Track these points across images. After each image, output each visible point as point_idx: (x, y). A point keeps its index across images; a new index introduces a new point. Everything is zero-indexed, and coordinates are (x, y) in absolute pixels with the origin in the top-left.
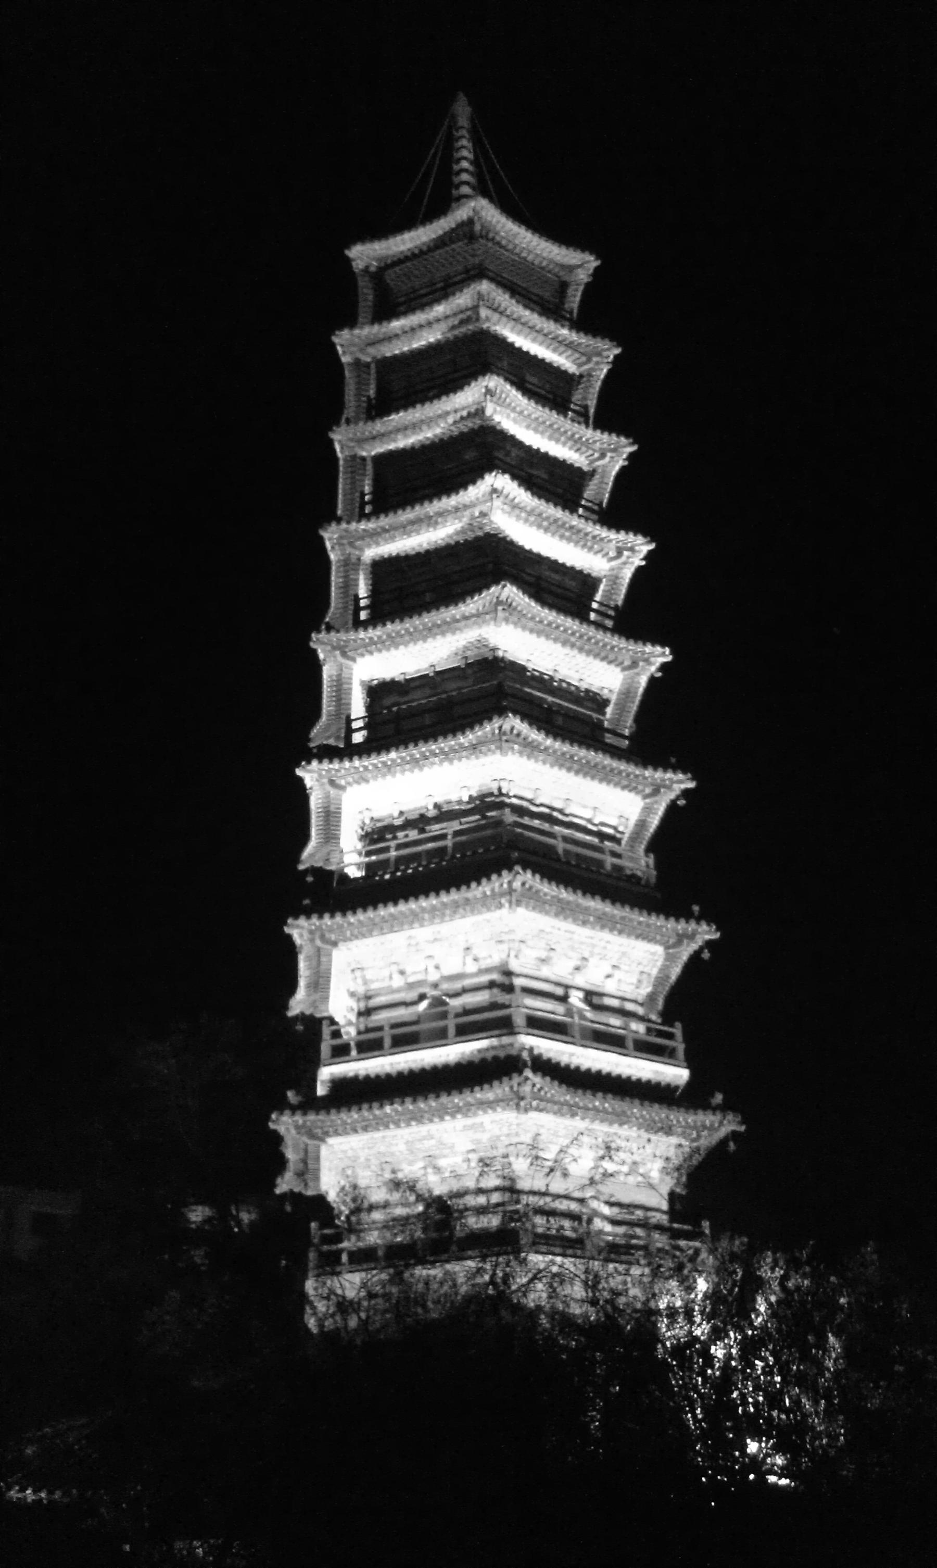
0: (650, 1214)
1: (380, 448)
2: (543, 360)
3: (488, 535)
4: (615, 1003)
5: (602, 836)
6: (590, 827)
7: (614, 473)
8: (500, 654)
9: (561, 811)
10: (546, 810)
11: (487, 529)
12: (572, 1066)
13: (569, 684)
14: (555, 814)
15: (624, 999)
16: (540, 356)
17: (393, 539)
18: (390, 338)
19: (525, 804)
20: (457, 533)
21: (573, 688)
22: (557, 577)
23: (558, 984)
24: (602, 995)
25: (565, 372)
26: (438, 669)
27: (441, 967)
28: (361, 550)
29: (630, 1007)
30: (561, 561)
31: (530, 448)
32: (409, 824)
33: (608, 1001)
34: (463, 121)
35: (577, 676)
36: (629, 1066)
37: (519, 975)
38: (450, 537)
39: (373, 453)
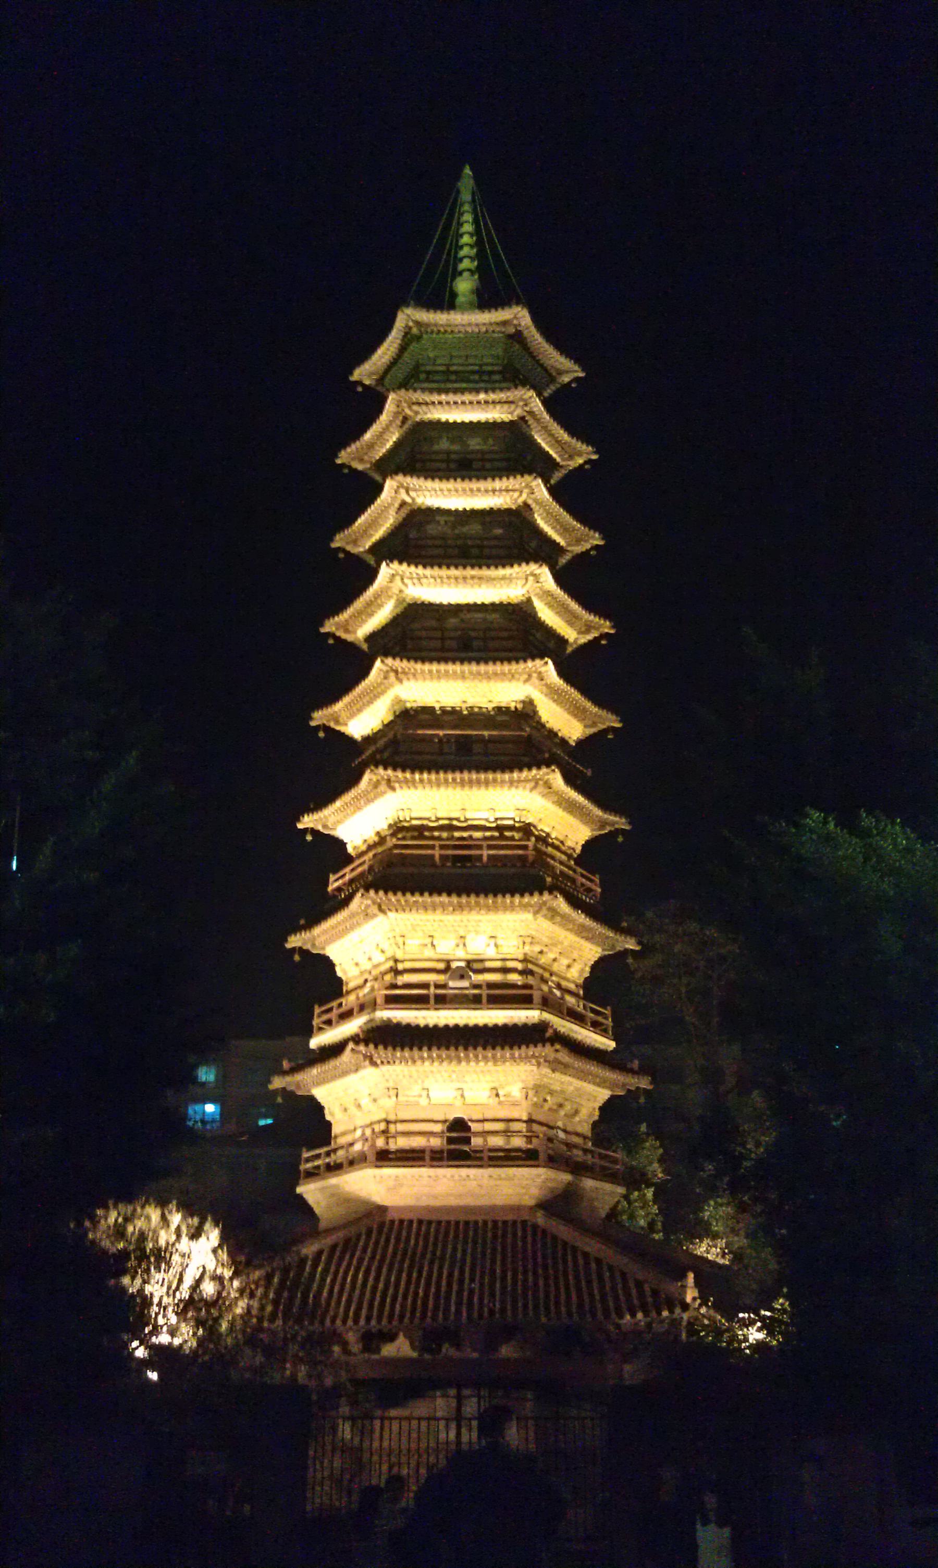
0: (511, 1124)
1: (368, 545)
2: (479, 422)
3: (410, 605)
4: (498, 964)
5: (501, 829)
6: (488, 825)
7: (548, 496)
8: (409, 705)
9: (458, 819)
10: (446, 822)
11: (408, 600)
12: (431, 1026)
13: (480, 708)
14: (455, 823)
15: (504, 960)
16: (475, 420)
17: (364, 621)
18: (371, 446)
19: (425, 822)
20: (396, 607)
21: (484, 710)
22: (480, 615)
23: (438, 961)
24: (482, 961)
25: (503, 423)
26: (385, 722)
27: (360, 963)
28: (355, 632)
29: (510, 964)
30: (479, 602)
31: (457, 511)
32: (441, 828)
33: (489, 964)
34: (466, 196)
35: (485, 700)
36: (482, 1017)
37: (402, 961)
38: (392, 611)
39: (367, 547)
